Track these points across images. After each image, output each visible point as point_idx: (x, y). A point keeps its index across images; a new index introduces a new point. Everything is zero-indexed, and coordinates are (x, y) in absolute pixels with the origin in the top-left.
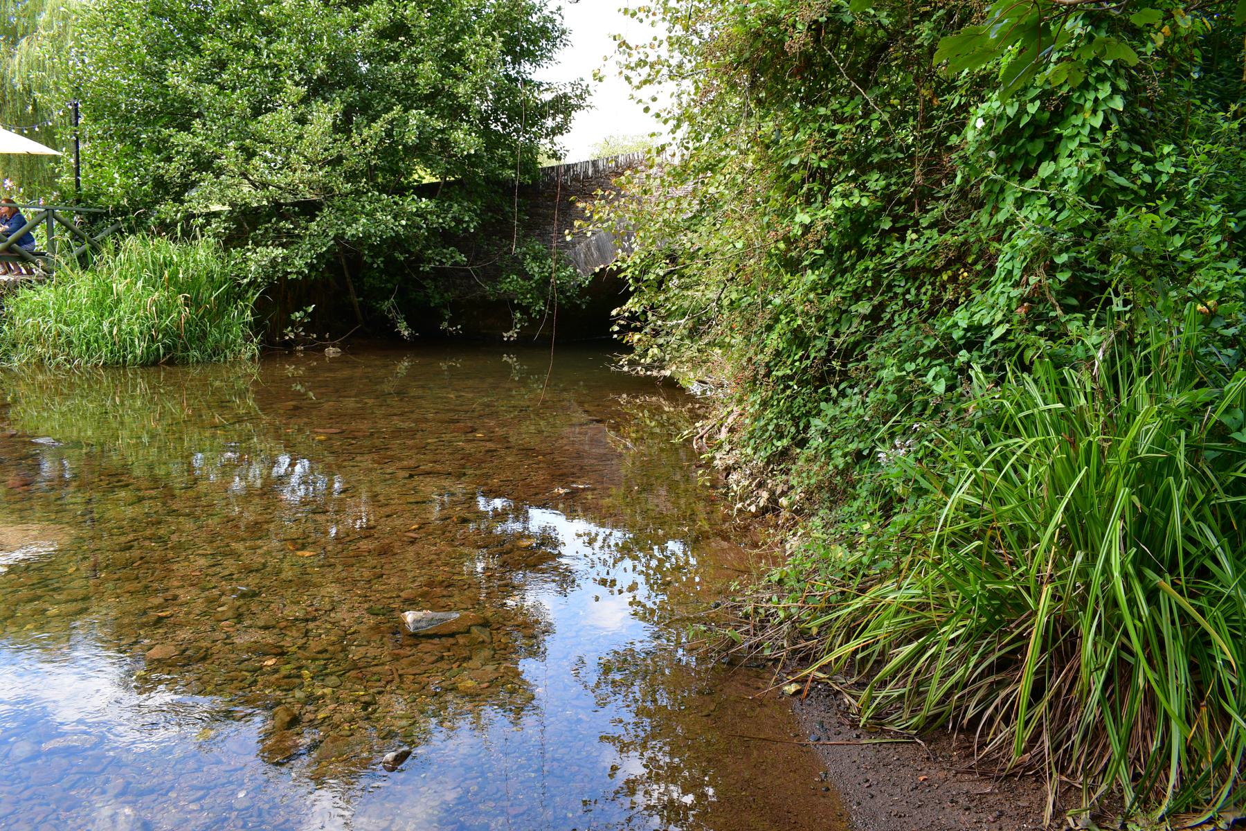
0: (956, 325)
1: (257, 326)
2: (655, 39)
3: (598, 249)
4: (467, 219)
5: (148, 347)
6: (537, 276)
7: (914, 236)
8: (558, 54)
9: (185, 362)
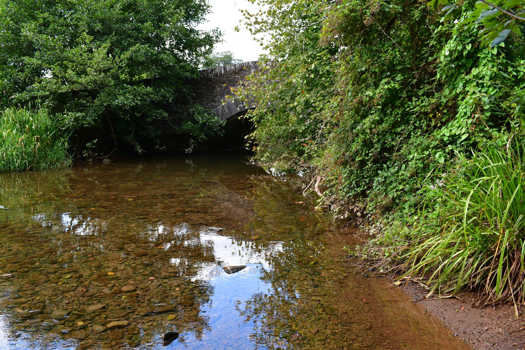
0: (444, 135)
1: (70, 151)
2: (260, 11)
3: (228, 108)
4: (168, 96)
5: (21, 162)
6: (201, 122)
7: (416, 99)
8: (206, 16)
9: (38, 169)
